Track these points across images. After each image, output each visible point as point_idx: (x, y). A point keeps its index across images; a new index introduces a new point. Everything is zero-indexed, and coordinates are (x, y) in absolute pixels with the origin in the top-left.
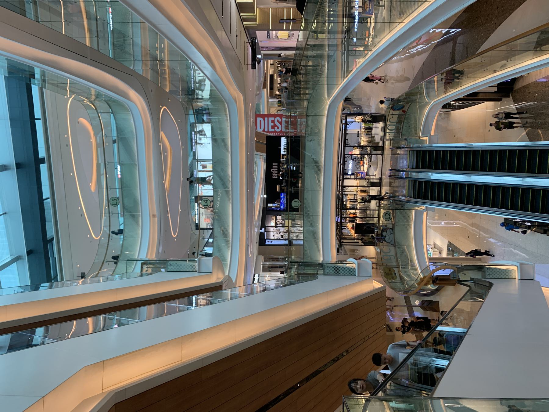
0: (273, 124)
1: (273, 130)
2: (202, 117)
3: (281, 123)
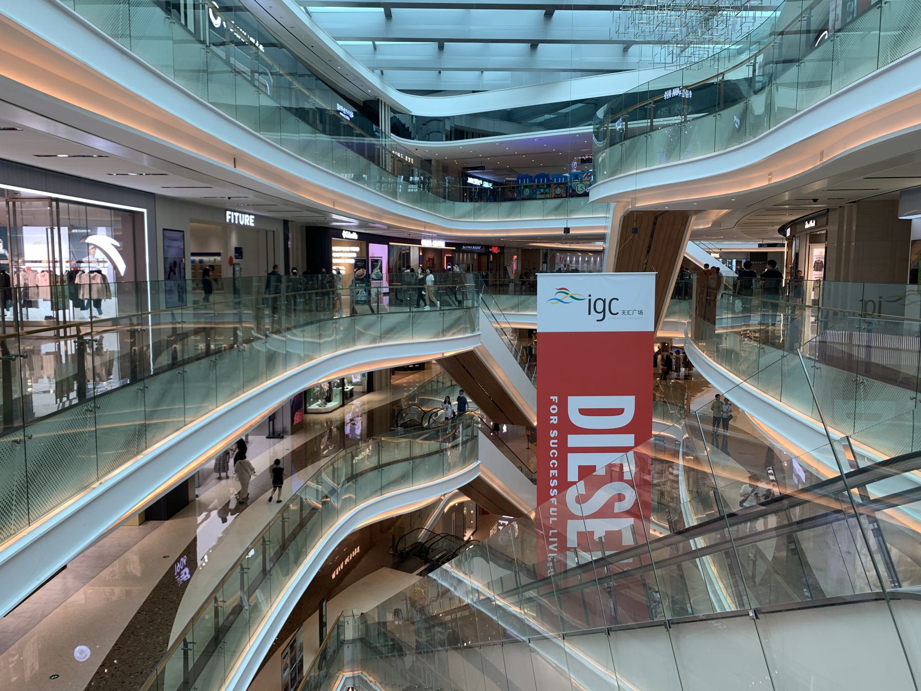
0: (601, 471)
1: (573, 475)
3: (605, 512)
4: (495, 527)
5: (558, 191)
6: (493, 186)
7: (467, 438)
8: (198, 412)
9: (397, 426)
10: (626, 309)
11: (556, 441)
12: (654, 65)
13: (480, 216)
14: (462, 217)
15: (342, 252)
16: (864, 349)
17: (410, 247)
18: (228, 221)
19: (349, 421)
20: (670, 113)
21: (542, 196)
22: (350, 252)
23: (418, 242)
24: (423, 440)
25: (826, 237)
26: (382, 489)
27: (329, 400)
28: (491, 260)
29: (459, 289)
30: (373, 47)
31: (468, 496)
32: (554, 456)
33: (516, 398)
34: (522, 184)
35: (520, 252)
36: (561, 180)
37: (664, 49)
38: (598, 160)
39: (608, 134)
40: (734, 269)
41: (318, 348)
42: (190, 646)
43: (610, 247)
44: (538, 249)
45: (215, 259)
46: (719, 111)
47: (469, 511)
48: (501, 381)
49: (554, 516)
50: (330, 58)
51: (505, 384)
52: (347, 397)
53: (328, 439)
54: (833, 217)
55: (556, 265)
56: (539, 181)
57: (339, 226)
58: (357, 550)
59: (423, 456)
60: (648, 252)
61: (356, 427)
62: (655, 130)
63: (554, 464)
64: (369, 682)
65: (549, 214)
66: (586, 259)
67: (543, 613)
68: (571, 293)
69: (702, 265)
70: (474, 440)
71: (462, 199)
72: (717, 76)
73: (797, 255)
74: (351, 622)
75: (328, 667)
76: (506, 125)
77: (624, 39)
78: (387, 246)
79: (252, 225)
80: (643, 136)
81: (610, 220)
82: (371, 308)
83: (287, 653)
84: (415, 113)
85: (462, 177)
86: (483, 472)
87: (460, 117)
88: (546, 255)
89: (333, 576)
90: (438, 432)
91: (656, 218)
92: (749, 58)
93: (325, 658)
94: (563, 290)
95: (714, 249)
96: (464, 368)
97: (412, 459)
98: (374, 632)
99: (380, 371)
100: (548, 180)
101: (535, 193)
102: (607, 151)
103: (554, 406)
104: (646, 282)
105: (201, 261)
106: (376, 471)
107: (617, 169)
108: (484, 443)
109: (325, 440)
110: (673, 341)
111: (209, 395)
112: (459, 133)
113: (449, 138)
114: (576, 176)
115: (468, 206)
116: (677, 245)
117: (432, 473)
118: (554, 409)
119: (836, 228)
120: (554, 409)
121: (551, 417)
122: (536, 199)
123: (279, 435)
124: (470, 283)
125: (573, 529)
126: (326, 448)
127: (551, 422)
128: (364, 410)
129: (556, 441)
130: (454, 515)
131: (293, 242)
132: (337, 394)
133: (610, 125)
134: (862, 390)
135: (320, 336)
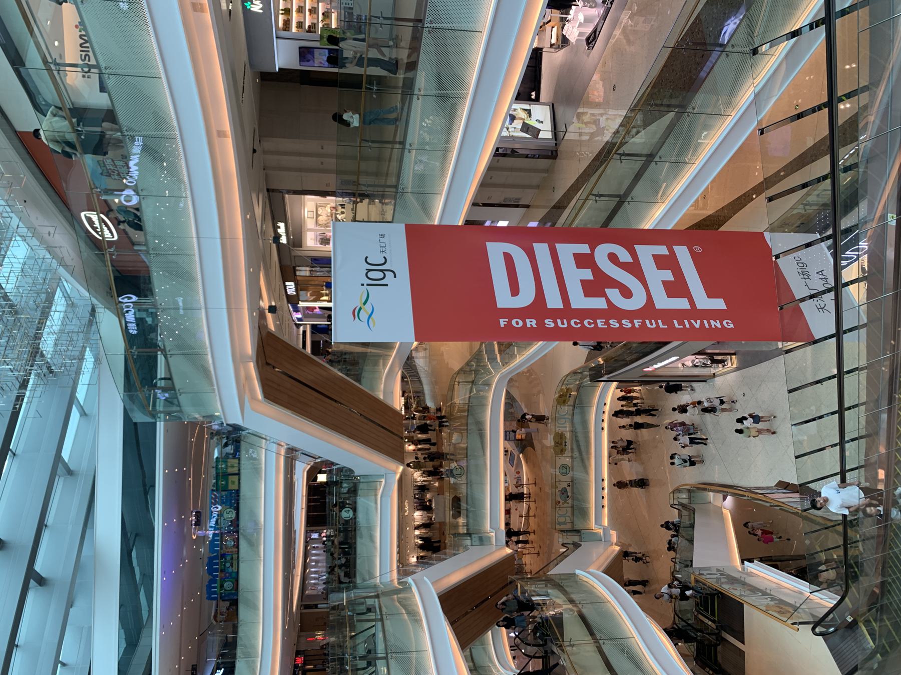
0: (587, 274)
1: (599, 303)
2: (856, 133)
3: (635, 269)
10: (379, 249)
11: (559, 321)
13: (254, 647)
49: (657, 324)
56: (216, 570)
66: (314, 564)
68: (359, 304)
69: (335, 338)
76: (140, 650)
88: (307, 607)
100: (215, 558)
101: (230, 574)
103: (514, 322)
118: (517, 323)
121: (529, 326)
122: (238, 573)
127: (535, 326)
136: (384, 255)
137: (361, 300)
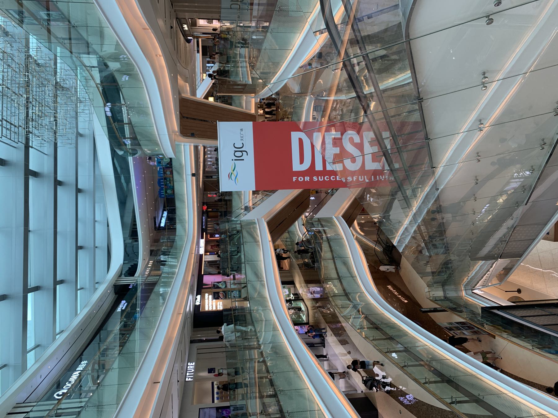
0: (337, 150)
3: (360, 147)
4: (372, 203)
5: (168, 173)
6: (166, 211)
7: (319, 225)
8: (312, 401)
9: (314, 267)
10: (240, 138)
12: (90, 121)
13: (185, 219)
14: (185, 230)
15: (208, 304)
16: (260, 7)
17: (204, 261)
18: (192, 380)
19: (312, 295)
20: (120, 112)
21: (172, 182)
22: (208, 299)
23: (201, 256)
24: (322, 252)
25: (193, 19)
26: (353, 277)
27: (300, 309)
28: (211, 210)
29: (229, 233)
30: (81, 290)
31: (355, 220)
32: (329, 178)
33: (294, 195)
34: (165, 194)
35: (206, 192)
36: (162, 171)
37: (81, 115)
38: (149, 153)
39: (134, 147)
40: (212, 65)
41: (268, 321)
42: (454, 400)
43: (201, 143)
44: (204, 182)
45: (216, 385)
46: (119, 85)
47: (363, 220)
48: (284, 205)
50: (89, 317)
51: (286, 202)
52: (298, 297)
53: (324, 308)
54: (181, 15)
55: (213, 170)
56: (163, 185)
57: (193, 306)
58: (390, 287)
59: (332, 251)
60: (204, 121)
61: (315, 290)
62: (130, 120)
63: (333, 178)
64: (468, 280)
65: (182, 178)
66: (209, 152)
67: (423, 182)
69: (221, 190)
70: (321, 221)
71: (174, 230)
72: (98, 88)
73: (204, 33)
74: (433, 293)
75: (459, 305)
76: (128, 205)
77: (75, 139)
78: (204, 276)
79: (194, 364)
80: (135, 129)
81: (186, 144)
82: (243, 288)
83: (454, 332)
84: (121, 261)
85: (160, 230)
86: (340, 213)
87: (124, 234)
88: (207, 177)
89: (406, 301)
90: (317, 243)
91: (184, 117)
92: (87, 70)
93: (455, 308)
94: (230, 176)
95: (201, 77)
96: (277, 226)
97: (333, 258)
98: (438, 278)
99: (281, 277)
101: (170, 187)
102: (144, 148)
104: (223, 127)
105: (217, 393)
106: (342, 280)
107: (153, 142)
108: (322, 214)
109: (324, 311)
110: (257, 102)
111: (299, 393)
112: (134, 234)
113: (136, 240)
114: (159, 163)
115: (178, 226)
116: (198, 104)
117: (342, 245)
119: (187, 14)
120: (301, 179)
121: (306, 180)
122: (173, 186)
123: (322, 340)
124: (227, 226)
125: (371, 166)
126: (329, 309)
127: (308, 180)
128: (305, 286)
129: (320, 177)
130: (365, 229)
131: (203, 337)
132: (296, 304)
133: (128, 147)
134: (284, 8)
135: (262, 321)
136: (243, 142)
137: (232, 169)
